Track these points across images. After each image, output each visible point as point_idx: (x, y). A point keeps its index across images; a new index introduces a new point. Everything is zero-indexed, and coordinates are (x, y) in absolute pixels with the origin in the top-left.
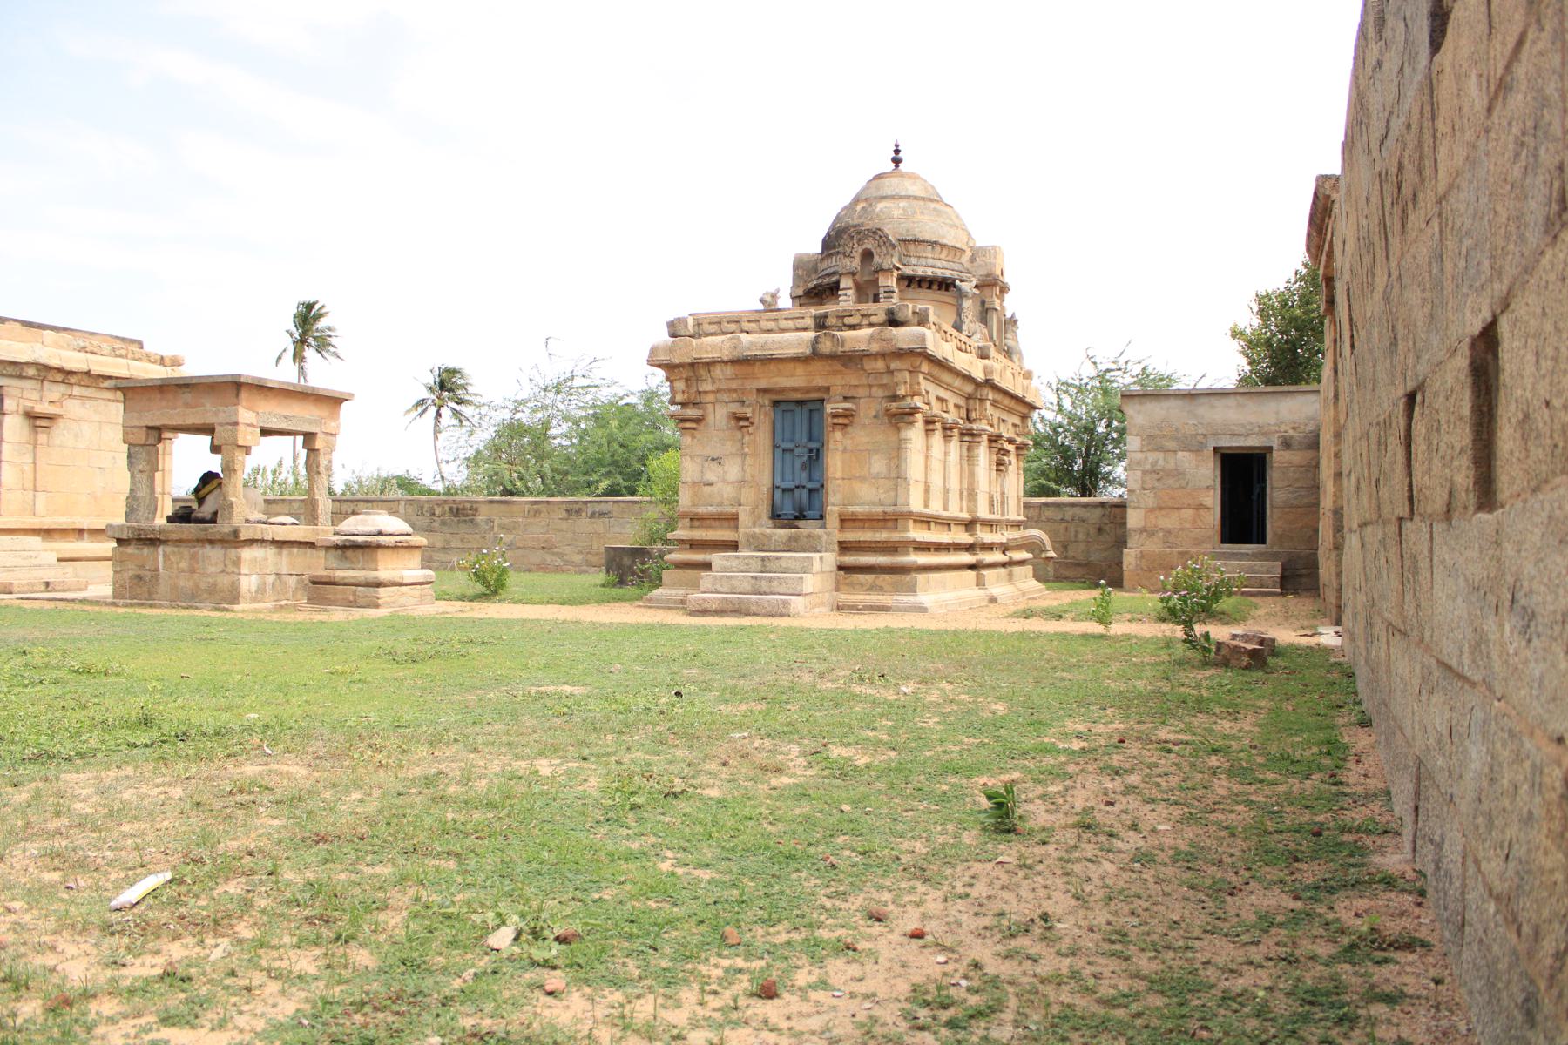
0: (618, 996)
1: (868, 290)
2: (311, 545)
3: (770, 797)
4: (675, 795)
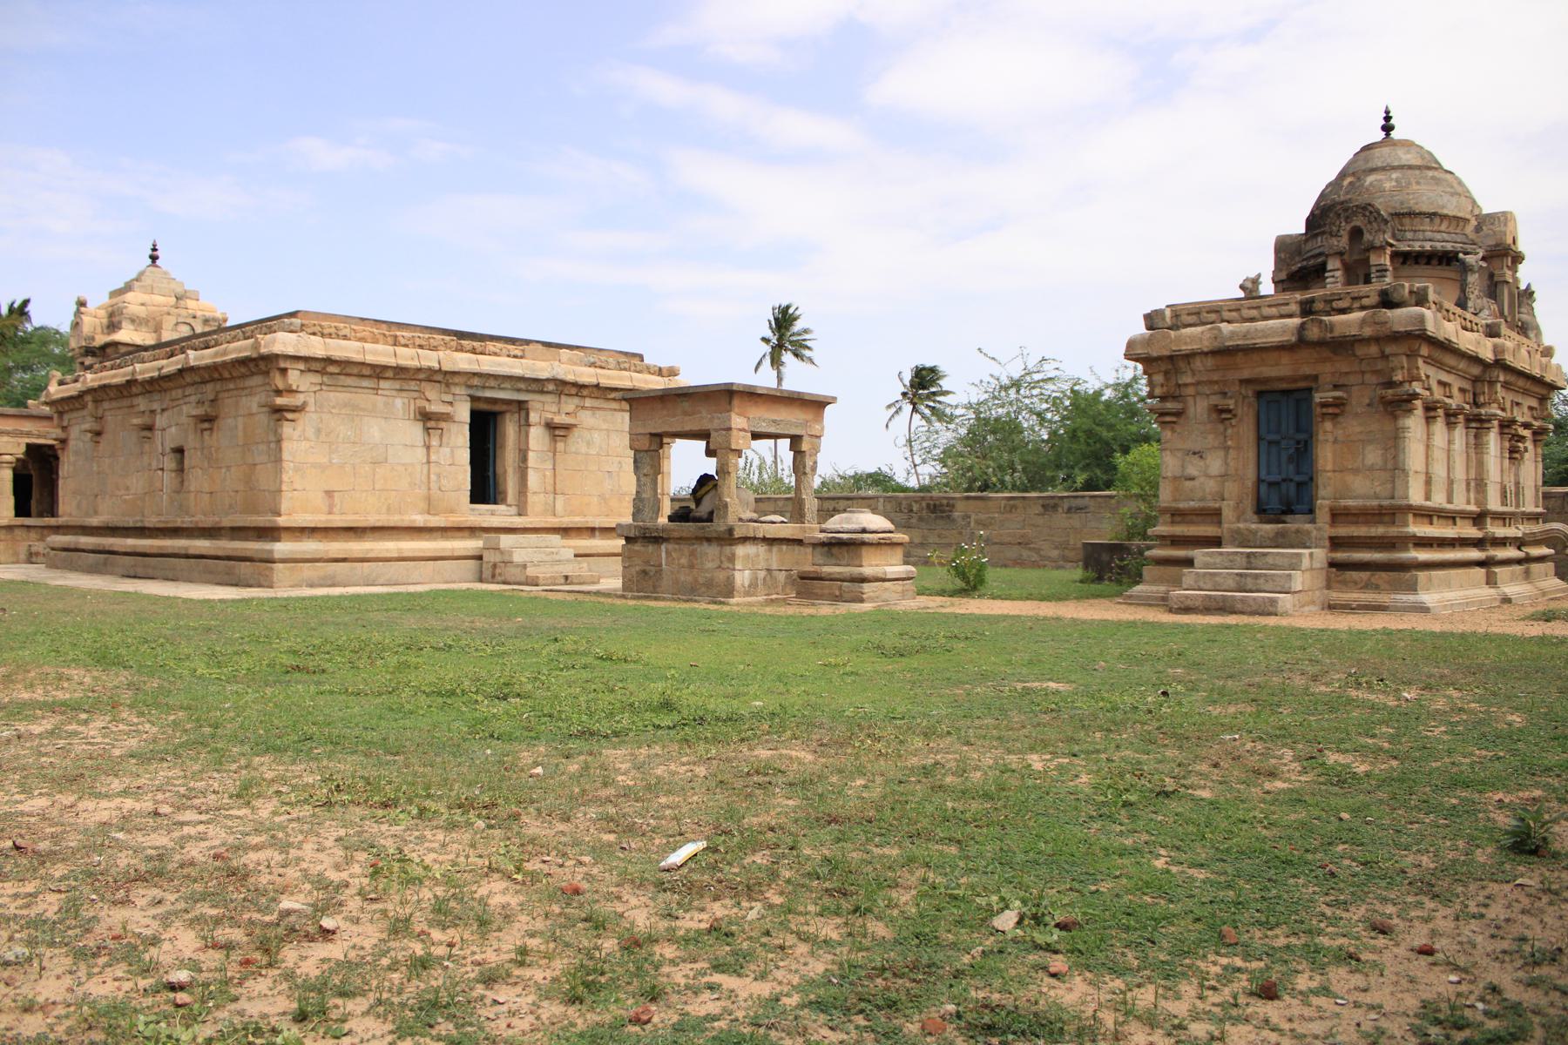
0: (1118, 984)
1: (1358, 271)
2: (799, 542)
3: (1263, 801)
4: (1167, 795)
